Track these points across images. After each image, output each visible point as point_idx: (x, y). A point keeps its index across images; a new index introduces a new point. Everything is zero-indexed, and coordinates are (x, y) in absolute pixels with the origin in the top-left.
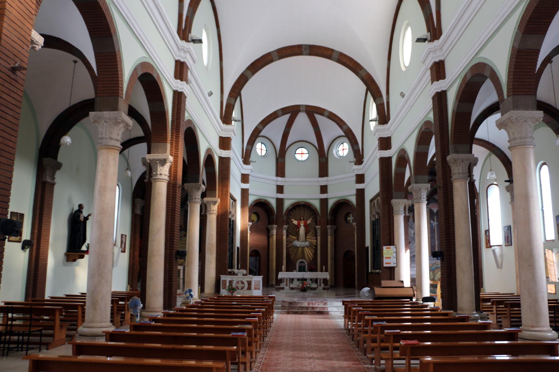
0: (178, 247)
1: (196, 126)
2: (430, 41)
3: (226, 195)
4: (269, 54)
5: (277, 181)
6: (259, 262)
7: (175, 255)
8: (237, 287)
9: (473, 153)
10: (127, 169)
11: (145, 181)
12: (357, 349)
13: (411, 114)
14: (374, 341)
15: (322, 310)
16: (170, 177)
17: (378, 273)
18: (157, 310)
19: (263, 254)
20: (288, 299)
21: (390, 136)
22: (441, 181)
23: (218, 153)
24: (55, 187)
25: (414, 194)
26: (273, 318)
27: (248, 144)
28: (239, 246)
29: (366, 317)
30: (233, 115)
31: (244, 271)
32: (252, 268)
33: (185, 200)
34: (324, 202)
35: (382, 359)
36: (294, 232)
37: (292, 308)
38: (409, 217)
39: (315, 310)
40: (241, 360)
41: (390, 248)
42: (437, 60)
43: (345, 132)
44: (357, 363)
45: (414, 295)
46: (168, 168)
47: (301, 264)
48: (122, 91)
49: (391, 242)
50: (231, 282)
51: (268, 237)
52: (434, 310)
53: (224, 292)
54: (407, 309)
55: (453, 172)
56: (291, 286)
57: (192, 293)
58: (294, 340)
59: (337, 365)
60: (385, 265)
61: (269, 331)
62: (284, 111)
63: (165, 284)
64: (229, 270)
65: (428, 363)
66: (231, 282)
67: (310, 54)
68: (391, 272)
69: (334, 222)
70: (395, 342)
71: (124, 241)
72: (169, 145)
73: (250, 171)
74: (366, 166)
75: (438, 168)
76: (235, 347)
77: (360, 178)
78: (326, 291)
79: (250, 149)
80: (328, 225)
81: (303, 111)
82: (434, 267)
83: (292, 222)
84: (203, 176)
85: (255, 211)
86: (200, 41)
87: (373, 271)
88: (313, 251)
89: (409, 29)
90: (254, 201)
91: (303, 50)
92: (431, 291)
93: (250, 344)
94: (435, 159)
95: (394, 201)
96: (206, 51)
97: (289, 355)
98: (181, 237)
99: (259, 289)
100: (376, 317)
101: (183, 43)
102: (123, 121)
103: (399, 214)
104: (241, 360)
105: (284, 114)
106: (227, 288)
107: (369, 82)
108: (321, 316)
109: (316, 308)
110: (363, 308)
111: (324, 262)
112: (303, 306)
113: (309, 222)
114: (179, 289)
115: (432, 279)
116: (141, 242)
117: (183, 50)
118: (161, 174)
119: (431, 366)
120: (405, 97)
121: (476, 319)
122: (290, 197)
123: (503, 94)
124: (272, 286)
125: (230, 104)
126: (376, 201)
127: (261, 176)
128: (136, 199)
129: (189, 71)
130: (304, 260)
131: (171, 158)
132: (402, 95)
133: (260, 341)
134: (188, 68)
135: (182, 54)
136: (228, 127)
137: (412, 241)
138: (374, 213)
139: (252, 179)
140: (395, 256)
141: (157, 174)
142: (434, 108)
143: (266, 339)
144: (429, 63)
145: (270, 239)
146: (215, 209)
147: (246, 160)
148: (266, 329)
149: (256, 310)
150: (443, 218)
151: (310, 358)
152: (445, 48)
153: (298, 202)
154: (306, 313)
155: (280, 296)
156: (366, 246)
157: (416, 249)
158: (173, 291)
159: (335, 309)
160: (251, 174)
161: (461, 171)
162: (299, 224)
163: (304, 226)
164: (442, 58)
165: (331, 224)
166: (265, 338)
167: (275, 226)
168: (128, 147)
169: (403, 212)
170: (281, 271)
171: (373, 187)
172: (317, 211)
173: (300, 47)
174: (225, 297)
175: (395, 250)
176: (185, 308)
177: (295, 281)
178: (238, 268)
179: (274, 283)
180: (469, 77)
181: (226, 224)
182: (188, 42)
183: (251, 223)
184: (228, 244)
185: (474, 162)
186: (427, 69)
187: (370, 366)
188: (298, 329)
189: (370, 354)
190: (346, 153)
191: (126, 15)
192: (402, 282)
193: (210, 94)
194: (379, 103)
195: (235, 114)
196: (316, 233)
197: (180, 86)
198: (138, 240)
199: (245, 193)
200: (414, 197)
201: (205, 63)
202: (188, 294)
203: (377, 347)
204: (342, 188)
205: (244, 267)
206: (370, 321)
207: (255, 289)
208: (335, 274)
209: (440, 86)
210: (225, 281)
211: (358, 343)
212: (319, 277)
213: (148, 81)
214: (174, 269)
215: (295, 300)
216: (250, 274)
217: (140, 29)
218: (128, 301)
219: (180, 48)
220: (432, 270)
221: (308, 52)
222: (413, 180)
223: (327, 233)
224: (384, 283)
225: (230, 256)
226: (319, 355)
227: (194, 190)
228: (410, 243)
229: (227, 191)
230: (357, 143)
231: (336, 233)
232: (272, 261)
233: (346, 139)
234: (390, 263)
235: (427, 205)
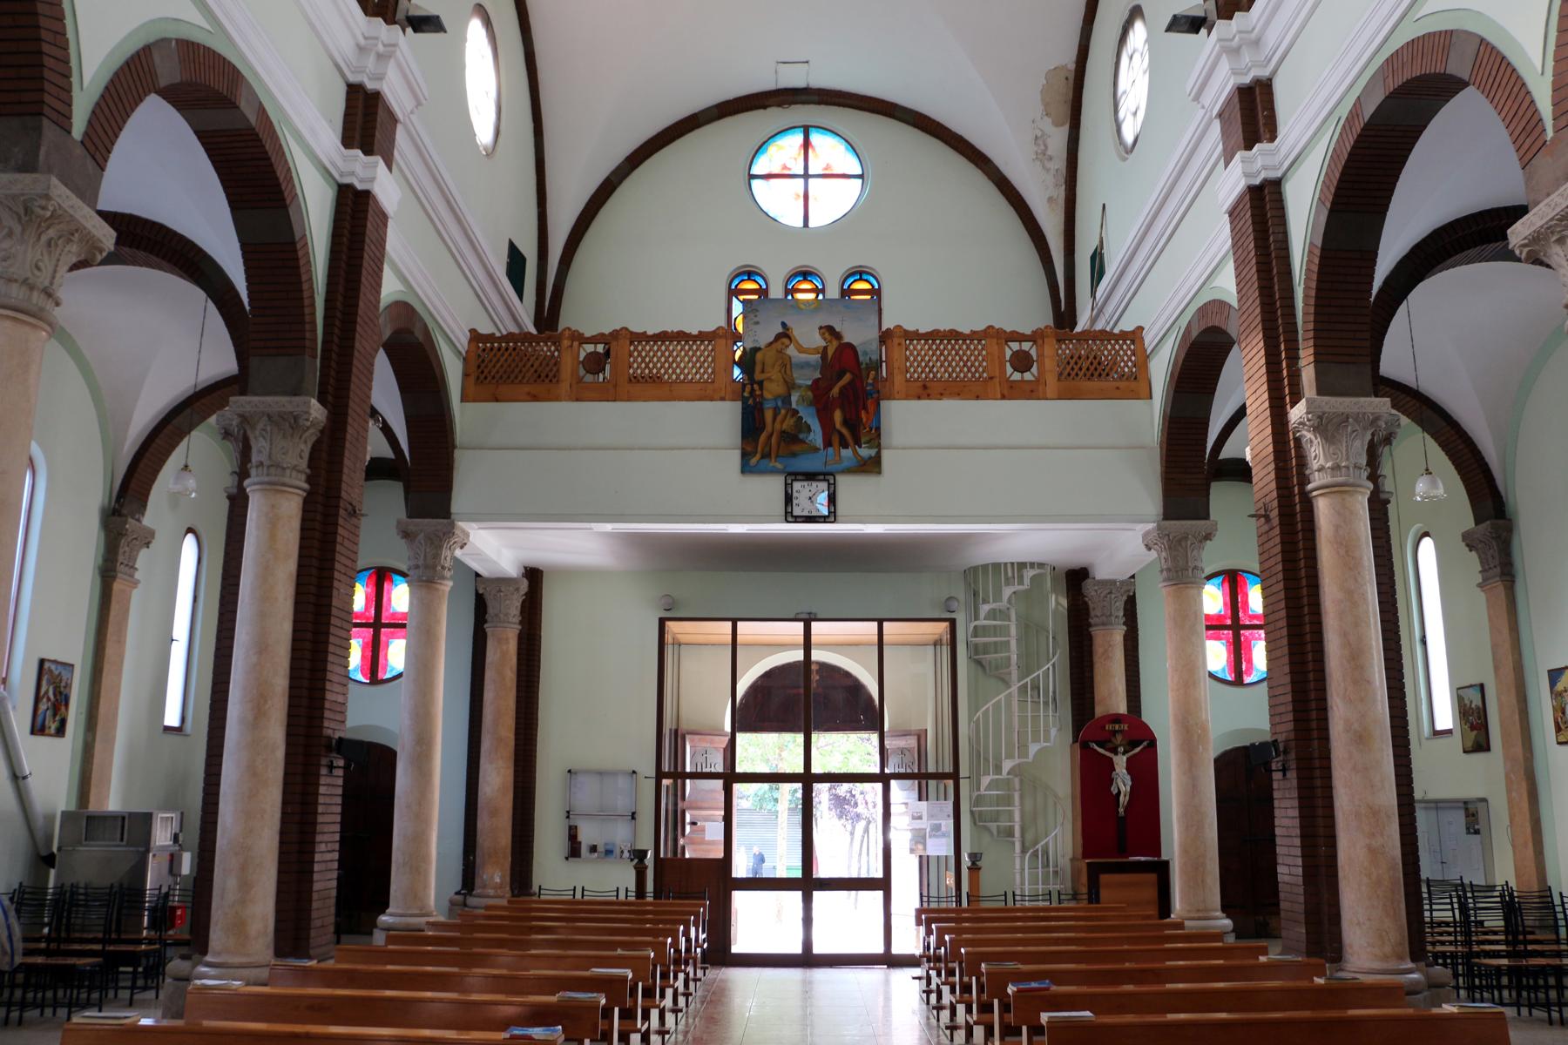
21: (1264, 73)
129: (399, 128)
131: (317, 411)
134: (394, 120)
142: (1236, 245)
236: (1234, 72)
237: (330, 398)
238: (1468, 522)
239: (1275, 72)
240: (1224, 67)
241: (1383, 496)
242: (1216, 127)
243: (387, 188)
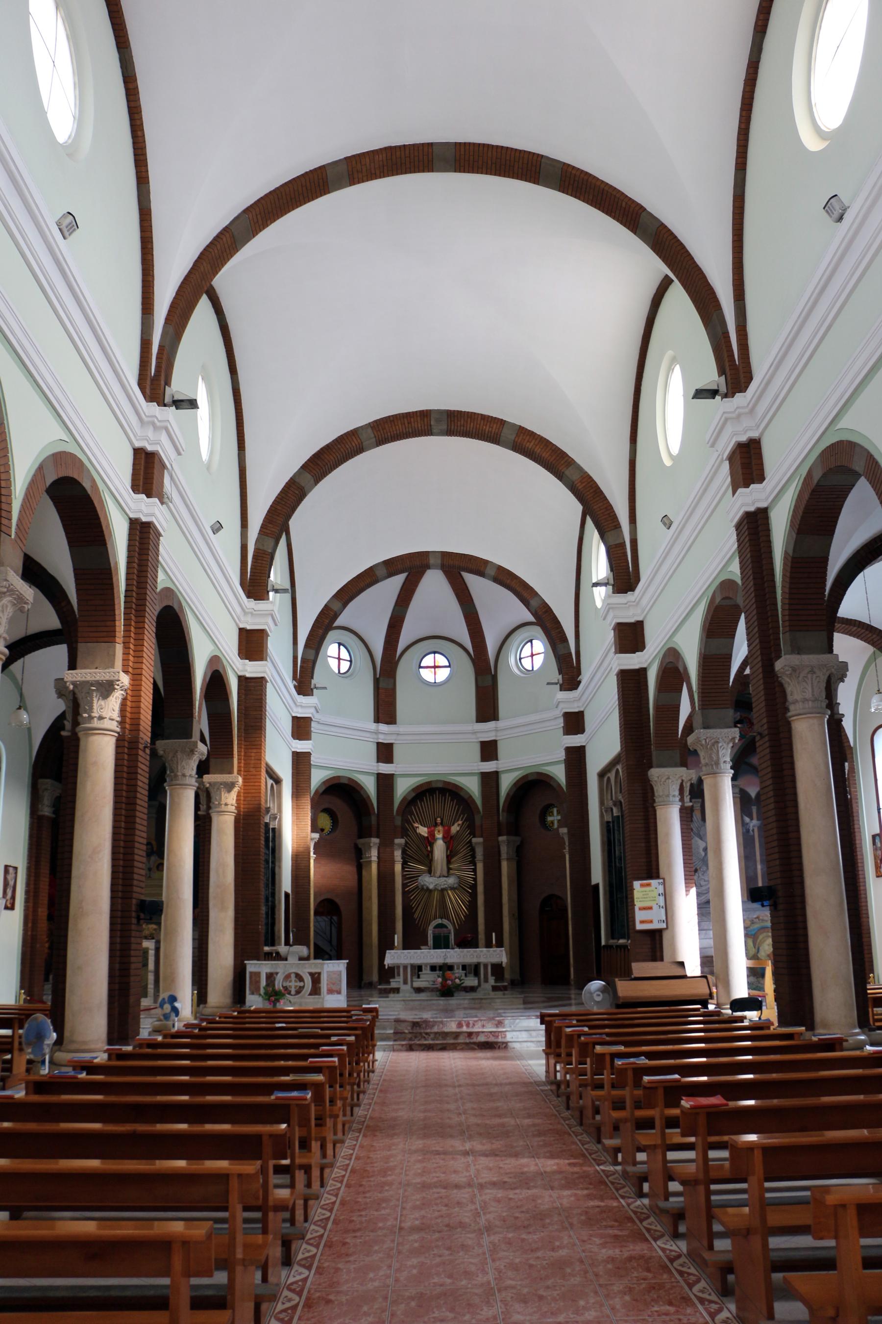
0: (141, 892)
1: (184, 604)
2: (726, 396)
3: (258, 767)
4: (353, 434)
5: (377, 733)
6: (339, 928)
7: (137, 912)
8: (286, 988)
9: (836, 649)
10: (20, 708)
11: (64, 733)
12: (579, 1129)
13: (689, 566)
14: (618, 1105)
15: (492, 1039)
16: (122, 723)
17: (624, 947)
18: (92, 1046)
19: (347, 909)
20: (410, 1016)
22: (765, 721)
23: (237, 668)
25: (702, 754)
26: (374, 1061)
27: (307, 646)
28: (289, 891)
29: (598, 1049)
30: (272, 577)
31: (303, 950)
32: (320, 943)
33: (160, 782)
34: (490, 780)
35: (640, 1149)
36: (420, 853)
37: (420, 1035)
38: (692, 809)
39: (475, 1040)
40: (298, 1161)
41: (649, 885)
42: (743, 438)
43: (535, 614)
44: (580, 1161)
45: (711, 996)
46: (119, 701)
47: (438, 931)
49: (651, 870)
50: (271, 977)
51: (360, 868)
52: (761, 1028)
53: (254, 1002)
54: (696, 1028)
55: (790, 698)
56: (418, 984)
57: (176, 1004)
58: (425, 1111)
59: (533, 1168)
60: (639, 927)
61: (364, 1092)
62: (391, 566)
63: (111, 982)
64: (266, 949)
65: (750, 1148)
66: (271, 977)
67: (450, 432)
68: (655, 943)
69: (514, 828)
70: (668, 1105)
71: (11, 883)
72: (119, 649)
73: (313, 710)
74: (587, 693)
75: (757, 692)
76: (284, 1126)
77: (574, 722)
78: (499, 994)
79: (312, 657)
80: (500, 835)
81: (435, 567)
82: (756, 926)
84: (202, 722)
85: (324, 807)
86: (192, 404)
87: (612, 942)
88: (467, 898)
89: (677, 369)
90: (324, 783)
91: (432, 423)
92: (750, 986)
93: (320, 1121)
94: (747, 671)
95: (655, 773)
96: (204, 431)
97: (414, 1148)
98: (150, 869)
99: (339, 992)
100: (622, 1048)
101: (153, 409)
102: (11, 591)
103: (667, 803)
104: (298, 1161)
105: (390, 575)
106: (262, 991)
108: (489, 1054)
109: (478, 1033)
110: (590, 1027)
111: (494, 923)
112: (446, 1030)
113: (455, 829)
114: (146, 996)
115: (752, 955)
116: (52, 884)
117: (153, 424)
118: (101, 718)
119: (758, 1155)
121: (860, 1046)
122: (409, 772)
124: (370, 985)
125: (264, 552)
126: (612, 775)
127: (339, 721)
128: (40, 781)
130: (445, 922)
132: (667, 522)
133: (345, 1115)
134: (164, 466)
135: (150, 433)
136: (261, 605)
137: (701, 867)
138: (611, 804)
139: (320, 728)
140: (662, 903)
141: (91, 718)
143: (359, 1112)
144: (726, 445)
145: (364, 873)
146: (229, 801)
147: (304, 682)
148: (359, 1086)
149: (334, 1039)
150: (772, 806)
151: (466, 1153)
152: (761, 409)
153: (429, 783)
154: (453, 1047)
155: (390, 1009)
156: (594, 882)
157: (712, 885)
158: (132, 1000)
159: (524, 1036)
160: (316, 717)
161: (808, 695)
162: (432, 834)
163: (444, 838)
164: (755, 434)
166: (356, 1109)
167: (375, 841)
168: (22, 655)
169: (677, 799)
170: (392, 947)
171: (604, 743)
172: (474, 801)
173: (425, 415)
174: (256, 1011)
175: (661, 889)
176: (160, 1038)
177: (426, 971)
178: (287, 943)
179: (375, 978)
180: (817, 475)
181: (257, 838)
182: (165, 405)
183: (316, 836)
184: (262, 885)
185: (839, 673)
186: (722, 461)
187: (611, 1168)
188: (434, 1084)
189: (611, 1138)
190: (539, 661)
191: (18, 341)
192: (682, 964)
193: (217, 528)
194: (612, 542)
195: (277, 575)
196: (473, 856)
197: (145, 508)
198: (45, 881)
199: (301, 762)
200: (703, 761)
201: (205, 454)
202: (167, 1007)
203: (625, 1120)
204: (531, 745)
205: (301, 939)
206: (608, 1058)
207: (330, 991)
208: (521, 954)
209: (752, 497)
210: (258, 974)
211: (581, 1113)
212: (483, 960)
213: (70, 496)
214: (133, 946)
215: (427, 1015)
216: (316, 958)
217: (52, 374)
218: (21, 1027)
219: (145, 419)
220: (751, 935)
221: (444, 427)
222: (698, 720)
223: (499, 855)
224: (639, 968)
225: (267, 914)
226: (487, 1147)
227: (179, 755)
228: (696, 871)
229: (259, 758)
230: (564, 639)
231: (520, 856)
232: (371, 924)
233: (537, 630)
234: (651, 922)
235: (734, 779)
237: (130, 670)
239: (645, 617)
241: (836, 717)
242: (726, 465)
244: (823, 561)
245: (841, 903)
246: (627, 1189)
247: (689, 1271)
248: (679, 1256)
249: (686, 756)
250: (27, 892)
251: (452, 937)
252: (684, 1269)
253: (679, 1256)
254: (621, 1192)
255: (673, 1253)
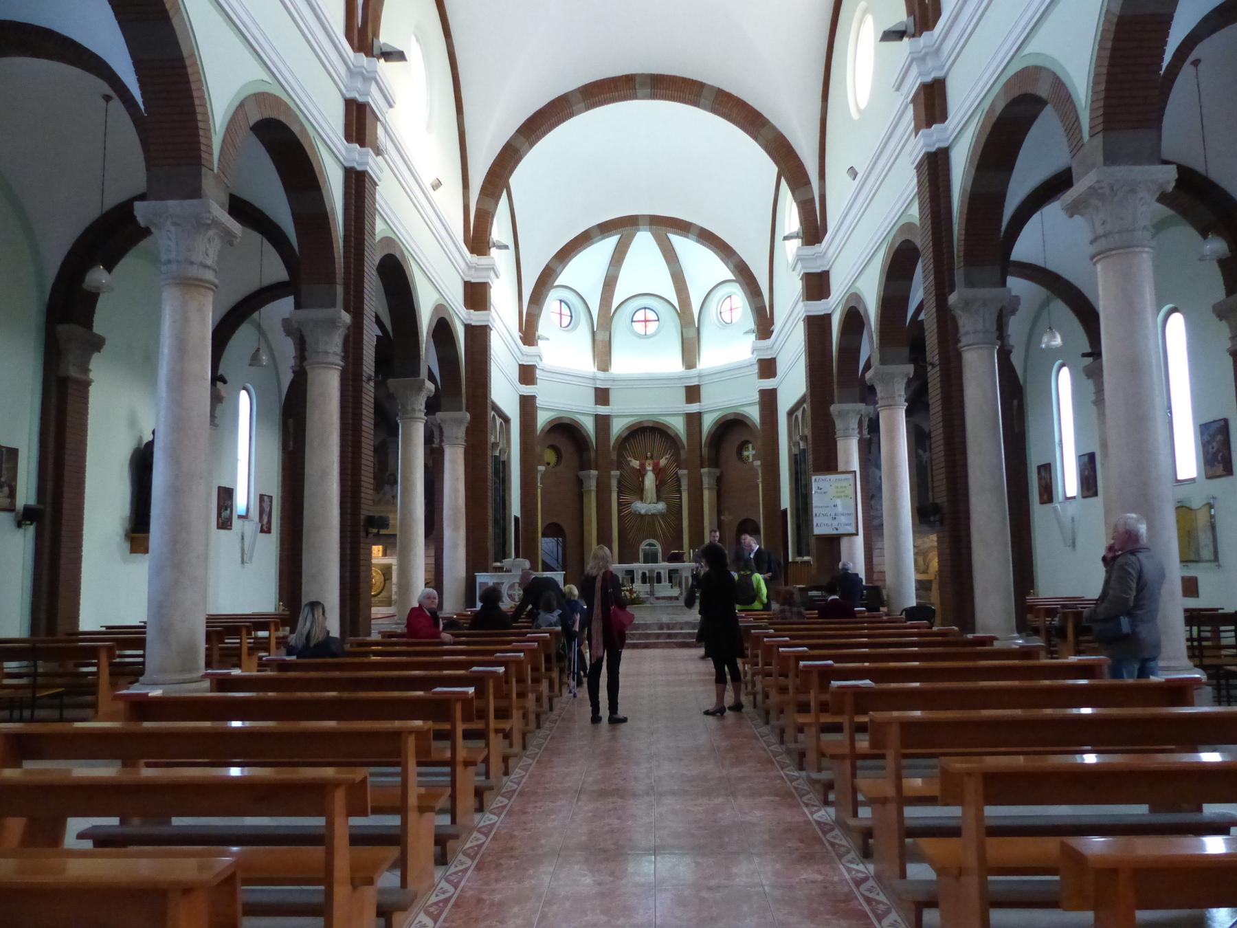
0: (368, 509)
2: (914, 36)
13: (873, 207)
21: (826, 269)
23: (461, 317)
24: (91, 389)
25: (878, 389)
28: (519, 515)
34: (694, 420)
42: (929, 79)
48: (211, 154)
55: (962, 330)
62: (605, 228)
69: (715, 461)
77: (767, 367)
83: (628, 463)
87: (799, 559)
102: (216, 223)
103: (847, 436)
107: (781, 151)
113: (663, 462)
120: (858, 178)
123: (1080, 131)
126: (799, 413)
131: (346, 318)
132: (853, 172)
134: (377, 118)
136: (482, 260)
142: (919, 193)
144: (913, 83)
163: (653, 470)
165: (709, 466)
171: (792, 385)
182: (373, 56)
193: (437, 185)
195: (499, 230)
196: (679, 486)
197: (356, 155)
199: (528, 405)
203: (810, 725)
209: (936, 136)
213: (279, 138)
231: (720, 484)
235: (909, 413)
236: (920, 74)
238: (1219, 293)
240: (914, 71)
242: (911, 107)
243: (374, 165)
244: (1001, 198)
245: (1004, 519)
246: (811, 795)
247: (877, 898)
248: (866, 879)
249: (868, 393)
250: (282, 518)
251: (660, 555)
252: (871, 895)
253: (866, 879)
254: (804, 799)
255: (860, 875)
